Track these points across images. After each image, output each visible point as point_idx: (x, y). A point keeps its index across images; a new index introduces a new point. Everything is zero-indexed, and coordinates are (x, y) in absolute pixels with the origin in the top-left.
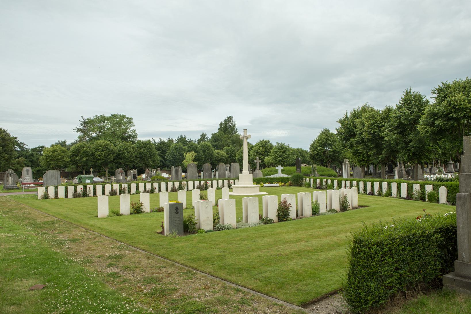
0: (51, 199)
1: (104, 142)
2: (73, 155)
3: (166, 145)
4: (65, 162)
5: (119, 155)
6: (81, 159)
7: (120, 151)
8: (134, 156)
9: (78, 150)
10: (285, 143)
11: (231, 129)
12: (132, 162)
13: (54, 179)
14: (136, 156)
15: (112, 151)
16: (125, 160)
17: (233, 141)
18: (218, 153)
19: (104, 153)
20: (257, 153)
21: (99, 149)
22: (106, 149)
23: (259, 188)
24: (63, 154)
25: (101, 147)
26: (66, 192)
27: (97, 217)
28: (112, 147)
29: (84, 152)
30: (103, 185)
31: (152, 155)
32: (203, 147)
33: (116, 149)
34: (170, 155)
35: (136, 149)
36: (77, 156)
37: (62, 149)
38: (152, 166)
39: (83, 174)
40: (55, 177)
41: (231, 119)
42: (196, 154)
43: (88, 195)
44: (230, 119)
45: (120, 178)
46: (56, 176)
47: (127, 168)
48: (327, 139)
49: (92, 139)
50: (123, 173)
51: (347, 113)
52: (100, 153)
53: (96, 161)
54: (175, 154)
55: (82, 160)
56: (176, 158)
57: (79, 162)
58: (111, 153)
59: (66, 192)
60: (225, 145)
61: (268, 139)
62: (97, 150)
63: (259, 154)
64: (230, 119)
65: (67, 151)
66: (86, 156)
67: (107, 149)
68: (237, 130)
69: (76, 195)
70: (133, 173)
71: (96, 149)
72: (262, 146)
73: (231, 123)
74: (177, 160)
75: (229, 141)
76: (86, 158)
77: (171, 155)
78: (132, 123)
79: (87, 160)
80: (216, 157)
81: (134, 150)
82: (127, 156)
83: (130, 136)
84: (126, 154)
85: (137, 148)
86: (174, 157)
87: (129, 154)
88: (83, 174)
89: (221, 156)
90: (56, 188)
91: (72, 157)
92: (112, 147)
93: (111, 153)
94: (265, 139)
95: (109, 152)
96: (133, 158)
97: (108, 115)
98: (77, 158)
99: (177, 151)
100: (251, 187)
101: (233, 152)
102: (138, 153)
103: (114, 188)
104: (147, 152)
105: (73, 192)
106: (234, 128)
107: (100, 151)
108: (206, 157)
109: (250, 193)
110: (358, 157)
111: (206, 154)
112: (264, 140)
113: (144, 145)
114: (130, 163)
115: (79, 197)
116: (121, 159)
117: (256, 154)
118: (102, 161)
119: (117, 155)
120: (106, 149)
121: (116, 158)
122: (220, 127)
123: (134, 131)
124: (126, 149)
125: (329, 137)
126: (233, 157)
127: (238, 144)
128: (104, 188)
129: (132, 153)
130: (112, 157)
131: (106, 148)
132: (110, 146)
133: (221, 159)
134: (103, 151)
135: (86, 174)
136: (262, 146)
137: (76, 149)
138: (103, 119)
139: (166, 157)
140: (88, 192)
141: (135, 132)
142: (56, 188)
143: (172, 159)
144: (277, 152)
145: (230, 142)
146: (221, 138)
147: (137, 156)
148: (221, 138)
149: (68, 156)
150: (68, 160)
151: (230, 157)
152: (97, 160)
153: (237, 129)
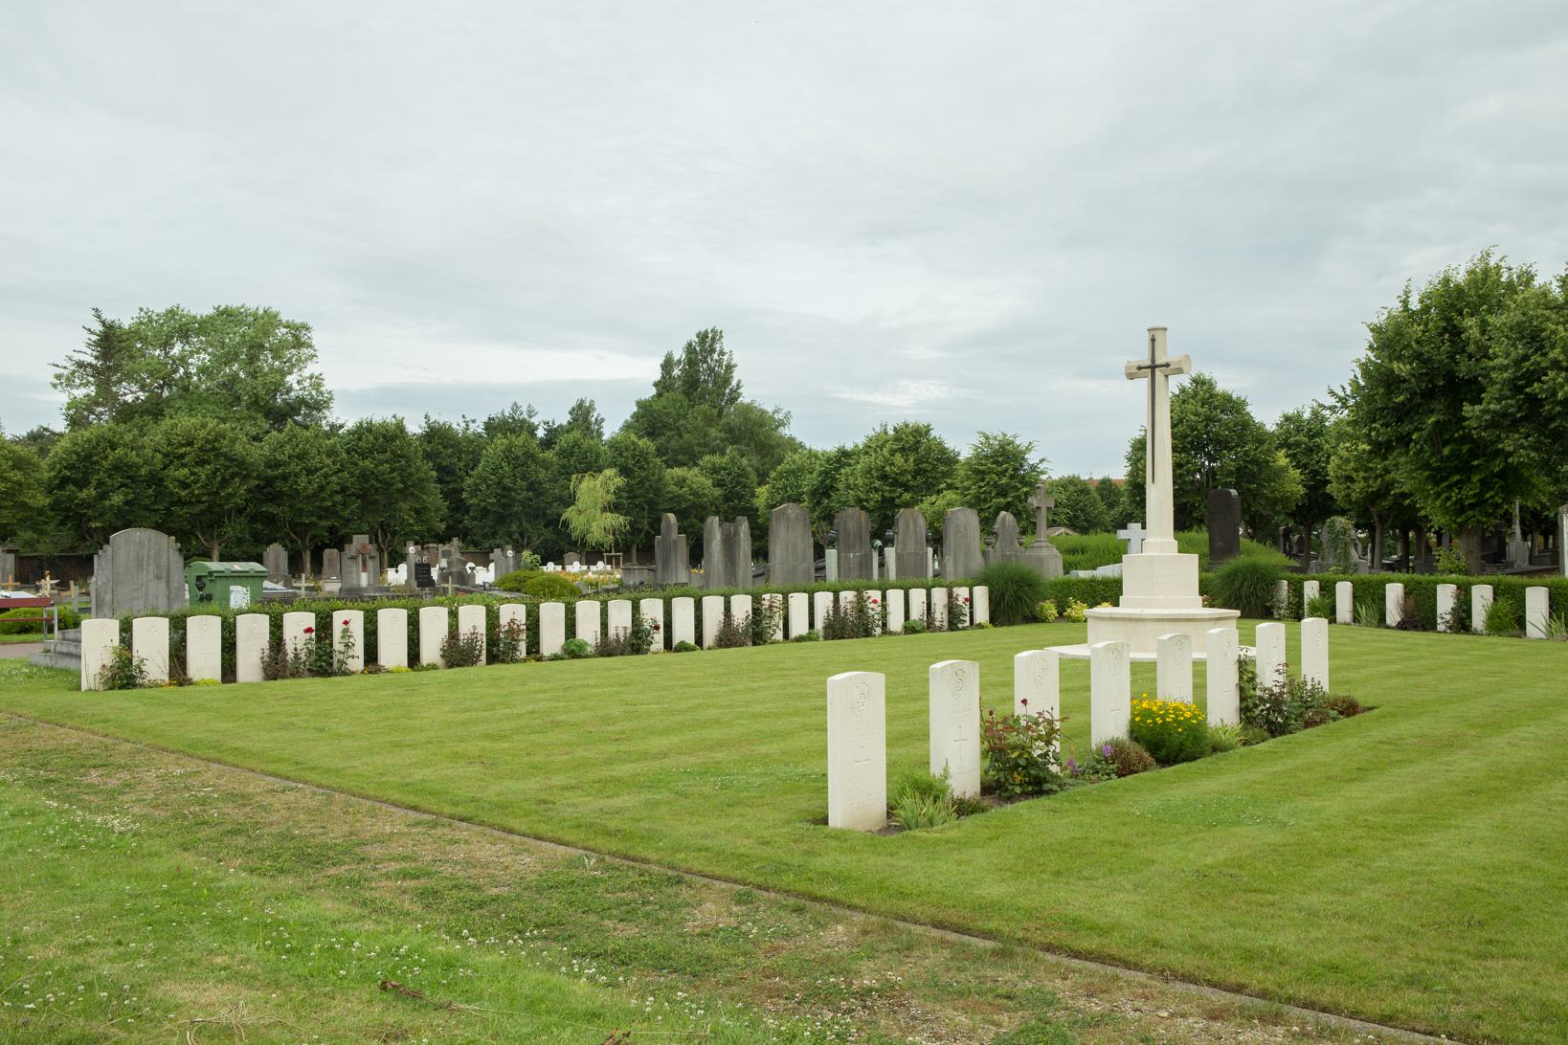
0: (156, 685)
1: (204, 426)
2: (64, 481)
3: (452, 446)
4: (30, 509)
5: (269, 481)
6: (104, 496)
7: (278, 465)
8: (338, 488)
9: (88, 457)
10: (1015, 437)
11: (715, 383)
12: (329, 513)
13: (151, 576)
14: (343, 490)
15: (241, 463)
16: (299, 505)
17: (730, 430)
18: (681, 482)
19: (204, 472)
20: (884, 477)
21: (182, 456)
22: (212, 455)
23: (1234, 622)
24: (17, 476)
25: (190, 444)
26: (229, 647)
27: (825, 821)
28: (238, 447)
29: (116, 468)
30: (366, 611)
31: (411, 488)
32: (621, 455)
33: (258, 453)
34: (483, 487)
35: (345, 455)
36: (82, 484)
37: (14, 452)
38: (412, 531)
39: (208, 556)
40: (158, 566)
41: (713, 339)
42: (620, 481)
43: (342, 662)
44: (705, 345)
45: (358, 578)
46: (163, 561)
47: (303, 539)
48: (1209, 419)
49: (126, 413)
50: (372, 558)
51: (1407, 293)
52: (186, 471)
53: (167, 509)
54: (507, 481)
55: (107, 503)
56: (513, 500)
57: (90, 512)
58: (234, 475)
59: (229, 647)
60: (696, 448)
61: (922, 422)
62: (172, 458)
63: (892, 485)
64: (705, 345)
65: (35, 460)
66: (122, 486)
67: (217, 456)
68: (738, 386)
69: (277, 665)
70: (418, 559)
71: (166, 455)
72: (903, 449)
73: (716, 356)
74: (517, 508)
75: (713, 432)
76: (126, 494)
77: (488, 486)
78: (310, 346)
79: (127, 503)
80: (671, 499)
81: (334, 463)
82: (305, 488)
83: (293, 408)
84: (303, 480)
85: (348, 452)
86: (503, 496)
87: (316, 478)
88: (212, 561)
89: (695, 494)
90: (178, 625)
91: (61, 486)
92: (238, 447)
93: (234, 475)
94: (911, 422)
95: (227, 468)
96: (330, 496)
97: (201, 307)
98: (84, 494)
99: (515, 468)
100: (1211, 620)
101: (739, 475)
102: (352, 475)
103: (465, 630)
104: (393, 470)
105: (266, 646)
106: (727, 381)
107: (184, 466)
108: (636, 497)
109: (1145, 651)
110: (1460, 489)
111: (634, 482)
112: (907, 426)
113: (375, 439)
114: (320, 518)
115: (295, 674)
116: (275, 498)
117: (877, 484)
118: (197, 509)
119: (262, 483)
120: (212, 455)
121: (258, 495)
122: (663, 377)
123: (317, 382)
124: (302, 457)
125: (1215, 408)
126: (741, 498)
127: (752, 444)
128: (414, 624)
129: (326, 476)
130: (239, 490)
131: (214, 449)
132: (233, 441)
133: (694, 506)
134: (202, 463)
135: (223, 558)
136: (903, 449)
137: (77, 454)
138: (181, 327)
139: (464, 495)
140: (338, 646)
141: (319, 385)
142: (178, 625)
143: (493, 504)
144: (983, 472)
145: (722, 435)
146: (675, 422)
147: (347, 488)
148: (675, 422)
149: (40, 482)
150: (42, 500)
151: (727, 498)
152: (172, 504)
153: (739, 382)
